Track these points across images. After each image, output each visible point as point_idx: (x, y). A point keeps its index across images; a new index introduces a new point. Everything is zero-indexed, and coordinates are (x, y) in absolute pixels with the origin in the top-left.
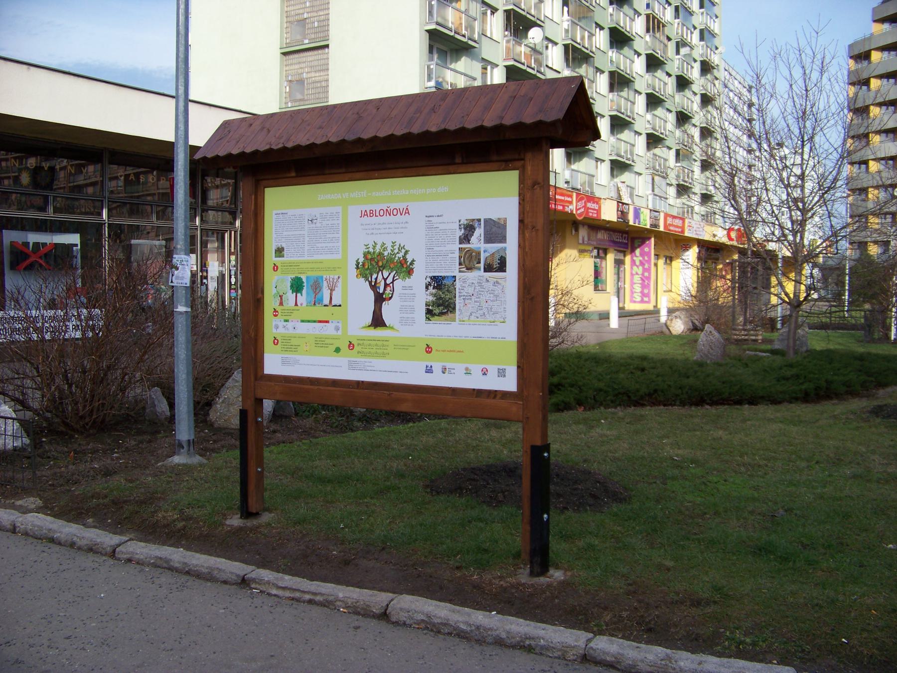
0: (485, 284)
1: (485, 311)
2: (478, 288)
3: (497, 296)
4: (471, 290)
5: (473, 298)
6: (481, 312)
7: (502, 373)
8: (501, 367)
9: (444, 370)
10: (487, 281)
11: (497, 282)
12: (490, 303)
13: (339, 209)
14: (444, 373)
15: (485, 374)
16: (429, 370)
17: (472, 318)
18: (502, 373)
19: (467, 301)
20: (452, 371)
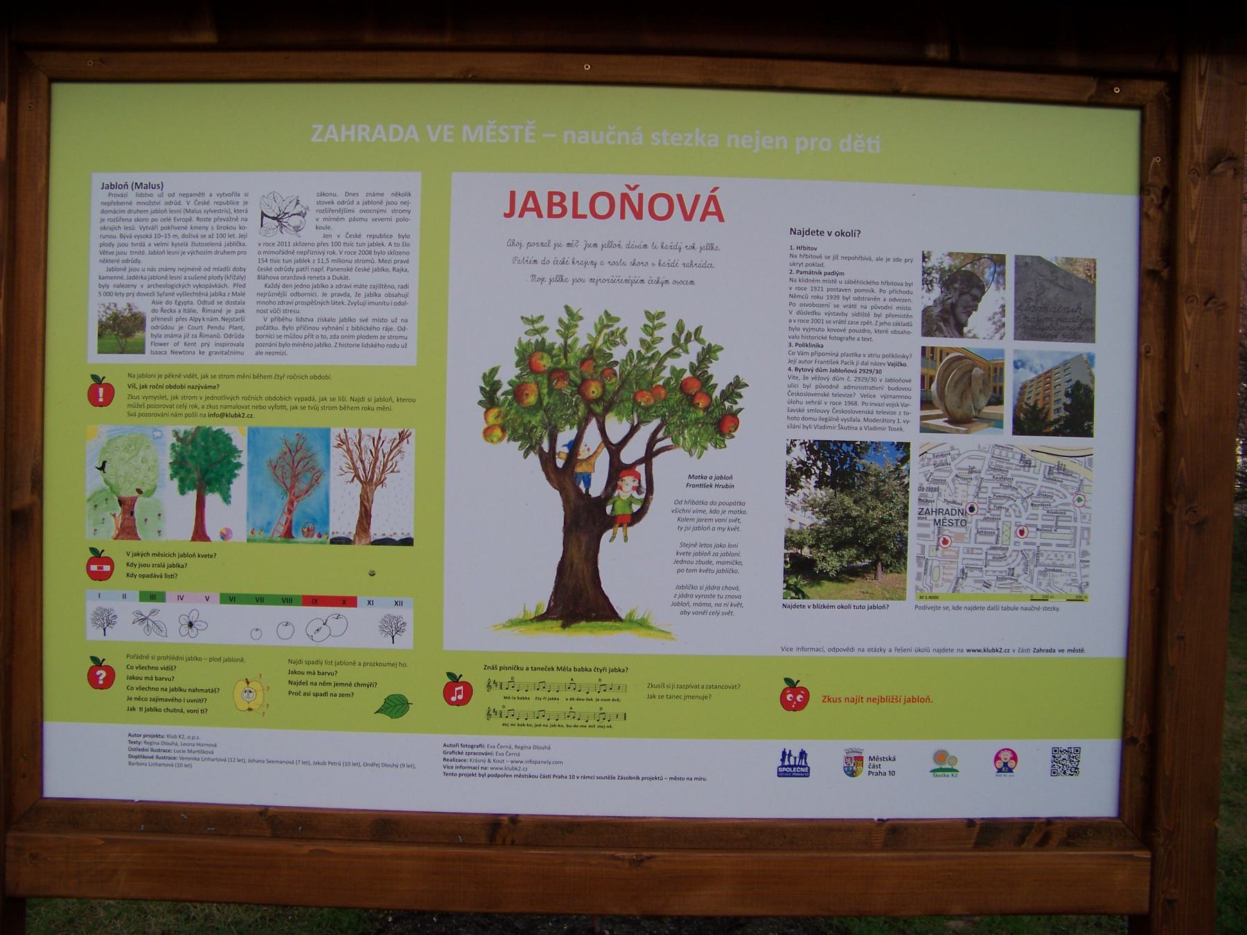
9: (853, 766)
14: (852, 773)
15: (1006, 769)
20: (886, 766)
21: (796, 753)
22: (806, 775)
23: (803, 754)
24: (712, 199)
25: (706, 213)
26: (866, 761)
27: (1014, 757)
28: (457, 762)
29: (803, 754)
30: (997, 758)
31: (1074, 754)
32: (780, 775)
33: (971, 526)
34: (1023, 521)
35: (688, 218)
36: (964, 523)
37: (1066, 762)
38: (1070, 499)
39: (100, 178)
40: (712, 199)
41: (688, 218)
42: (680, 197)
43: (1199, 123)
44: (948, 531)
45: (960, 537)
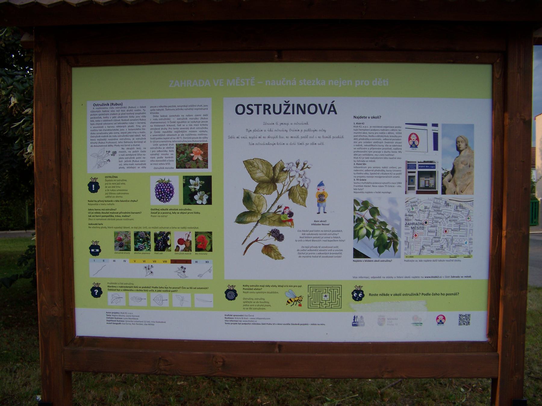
0: (443, 209)
1: (443, 242)
2: (433, 214)
3: (460, 224)
4: (423, 217)
5: (426, 226)
6: (438, 245)
7: (464, 320)
10: (447, 204)
11: (461, 206)
12: (450, 232)
14: (381, 325)
15: (441, 323)
17: (425, 252)
19: (416, 231)
24: (332, 105)
26: (386, 320)
27: (444, 318)
30: (437, 318)
31: (468, 317)
33: (426, 229)
35: (323, 113)
36: (423, 228)
37: (464, 320)
40: (332, 105)
41: (323, 113)
42: (320, 105)
44: (416, 231)
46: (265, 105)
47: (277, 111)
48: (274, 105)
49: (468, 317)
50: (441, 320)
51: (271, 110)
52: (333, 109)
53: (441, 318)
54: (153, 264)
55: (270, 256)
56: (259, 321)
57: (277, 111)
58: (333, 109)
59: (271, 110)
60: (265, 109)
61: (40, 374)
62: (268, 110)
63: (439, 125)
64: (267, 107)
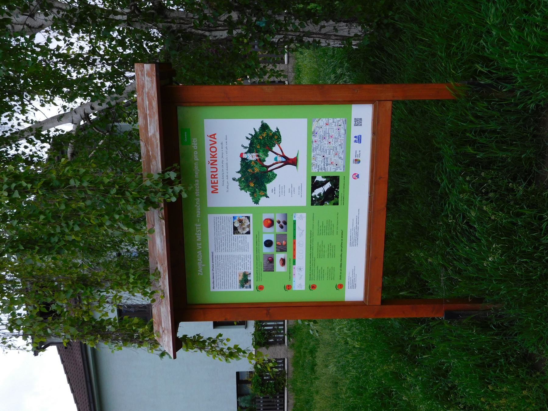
5: (326, 156)
8: (353, 123)
9: (357, 161)
13: (211, 218)
14: (359, 161)
15: (358, 176)
16: (359, 139)
18: (358, 122)
20: (358, 153)
21: (355, 139)
22: (361, 136)
23: (355, 137)
24: (210, 136)
25: (214, 138)
26: (357, 158)
27: (355, 174)
28: (355, 243)
29: (355, 137)
30: (355, 179)
31: (356, 120)
32: (360, 143)
33: (328, 156)
34: (327, 142)
35: (216, 143)
36: (327, 158)
37: (358, 122)
38: (321, 130)
39: (212, 290)
40: (210, 136)
41: (216, 143)
42: (210, 145)
43: (401, 293)
44: (329, 162)
45: (331, 159)
46: (212, 178)
47: (215, 170)
48: (212, 172)
49: (356, 120)
50: (356, 176)
51: (215, 174)
52: (213, 136)
53: (354, 176)
54: (26, 347)
55: (383, 277)
56: (355, 226)
57: (215, 170)
58: (213, 136)
59: (215, 174)
60: (214, 178)
61: (223, 37)
62: (215, 176)
63: (299, 162)
64: (213, 176)
